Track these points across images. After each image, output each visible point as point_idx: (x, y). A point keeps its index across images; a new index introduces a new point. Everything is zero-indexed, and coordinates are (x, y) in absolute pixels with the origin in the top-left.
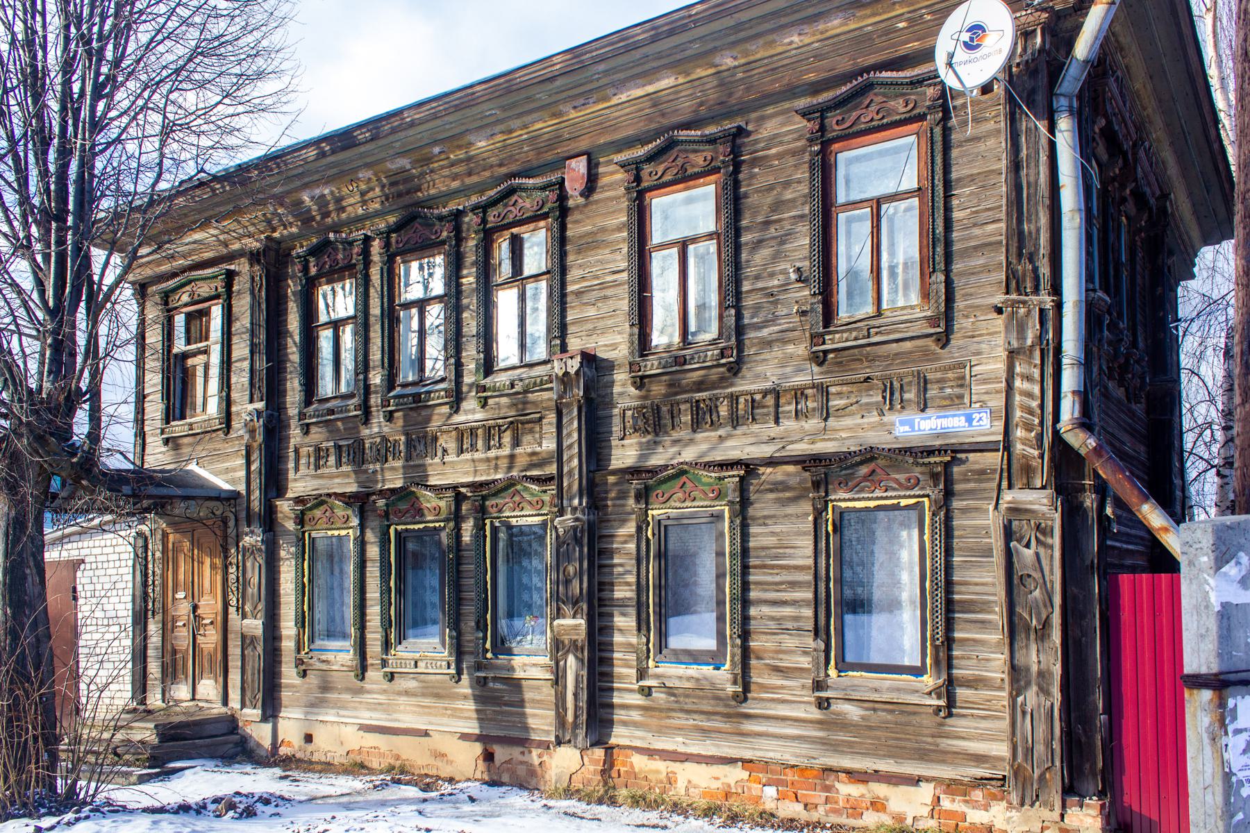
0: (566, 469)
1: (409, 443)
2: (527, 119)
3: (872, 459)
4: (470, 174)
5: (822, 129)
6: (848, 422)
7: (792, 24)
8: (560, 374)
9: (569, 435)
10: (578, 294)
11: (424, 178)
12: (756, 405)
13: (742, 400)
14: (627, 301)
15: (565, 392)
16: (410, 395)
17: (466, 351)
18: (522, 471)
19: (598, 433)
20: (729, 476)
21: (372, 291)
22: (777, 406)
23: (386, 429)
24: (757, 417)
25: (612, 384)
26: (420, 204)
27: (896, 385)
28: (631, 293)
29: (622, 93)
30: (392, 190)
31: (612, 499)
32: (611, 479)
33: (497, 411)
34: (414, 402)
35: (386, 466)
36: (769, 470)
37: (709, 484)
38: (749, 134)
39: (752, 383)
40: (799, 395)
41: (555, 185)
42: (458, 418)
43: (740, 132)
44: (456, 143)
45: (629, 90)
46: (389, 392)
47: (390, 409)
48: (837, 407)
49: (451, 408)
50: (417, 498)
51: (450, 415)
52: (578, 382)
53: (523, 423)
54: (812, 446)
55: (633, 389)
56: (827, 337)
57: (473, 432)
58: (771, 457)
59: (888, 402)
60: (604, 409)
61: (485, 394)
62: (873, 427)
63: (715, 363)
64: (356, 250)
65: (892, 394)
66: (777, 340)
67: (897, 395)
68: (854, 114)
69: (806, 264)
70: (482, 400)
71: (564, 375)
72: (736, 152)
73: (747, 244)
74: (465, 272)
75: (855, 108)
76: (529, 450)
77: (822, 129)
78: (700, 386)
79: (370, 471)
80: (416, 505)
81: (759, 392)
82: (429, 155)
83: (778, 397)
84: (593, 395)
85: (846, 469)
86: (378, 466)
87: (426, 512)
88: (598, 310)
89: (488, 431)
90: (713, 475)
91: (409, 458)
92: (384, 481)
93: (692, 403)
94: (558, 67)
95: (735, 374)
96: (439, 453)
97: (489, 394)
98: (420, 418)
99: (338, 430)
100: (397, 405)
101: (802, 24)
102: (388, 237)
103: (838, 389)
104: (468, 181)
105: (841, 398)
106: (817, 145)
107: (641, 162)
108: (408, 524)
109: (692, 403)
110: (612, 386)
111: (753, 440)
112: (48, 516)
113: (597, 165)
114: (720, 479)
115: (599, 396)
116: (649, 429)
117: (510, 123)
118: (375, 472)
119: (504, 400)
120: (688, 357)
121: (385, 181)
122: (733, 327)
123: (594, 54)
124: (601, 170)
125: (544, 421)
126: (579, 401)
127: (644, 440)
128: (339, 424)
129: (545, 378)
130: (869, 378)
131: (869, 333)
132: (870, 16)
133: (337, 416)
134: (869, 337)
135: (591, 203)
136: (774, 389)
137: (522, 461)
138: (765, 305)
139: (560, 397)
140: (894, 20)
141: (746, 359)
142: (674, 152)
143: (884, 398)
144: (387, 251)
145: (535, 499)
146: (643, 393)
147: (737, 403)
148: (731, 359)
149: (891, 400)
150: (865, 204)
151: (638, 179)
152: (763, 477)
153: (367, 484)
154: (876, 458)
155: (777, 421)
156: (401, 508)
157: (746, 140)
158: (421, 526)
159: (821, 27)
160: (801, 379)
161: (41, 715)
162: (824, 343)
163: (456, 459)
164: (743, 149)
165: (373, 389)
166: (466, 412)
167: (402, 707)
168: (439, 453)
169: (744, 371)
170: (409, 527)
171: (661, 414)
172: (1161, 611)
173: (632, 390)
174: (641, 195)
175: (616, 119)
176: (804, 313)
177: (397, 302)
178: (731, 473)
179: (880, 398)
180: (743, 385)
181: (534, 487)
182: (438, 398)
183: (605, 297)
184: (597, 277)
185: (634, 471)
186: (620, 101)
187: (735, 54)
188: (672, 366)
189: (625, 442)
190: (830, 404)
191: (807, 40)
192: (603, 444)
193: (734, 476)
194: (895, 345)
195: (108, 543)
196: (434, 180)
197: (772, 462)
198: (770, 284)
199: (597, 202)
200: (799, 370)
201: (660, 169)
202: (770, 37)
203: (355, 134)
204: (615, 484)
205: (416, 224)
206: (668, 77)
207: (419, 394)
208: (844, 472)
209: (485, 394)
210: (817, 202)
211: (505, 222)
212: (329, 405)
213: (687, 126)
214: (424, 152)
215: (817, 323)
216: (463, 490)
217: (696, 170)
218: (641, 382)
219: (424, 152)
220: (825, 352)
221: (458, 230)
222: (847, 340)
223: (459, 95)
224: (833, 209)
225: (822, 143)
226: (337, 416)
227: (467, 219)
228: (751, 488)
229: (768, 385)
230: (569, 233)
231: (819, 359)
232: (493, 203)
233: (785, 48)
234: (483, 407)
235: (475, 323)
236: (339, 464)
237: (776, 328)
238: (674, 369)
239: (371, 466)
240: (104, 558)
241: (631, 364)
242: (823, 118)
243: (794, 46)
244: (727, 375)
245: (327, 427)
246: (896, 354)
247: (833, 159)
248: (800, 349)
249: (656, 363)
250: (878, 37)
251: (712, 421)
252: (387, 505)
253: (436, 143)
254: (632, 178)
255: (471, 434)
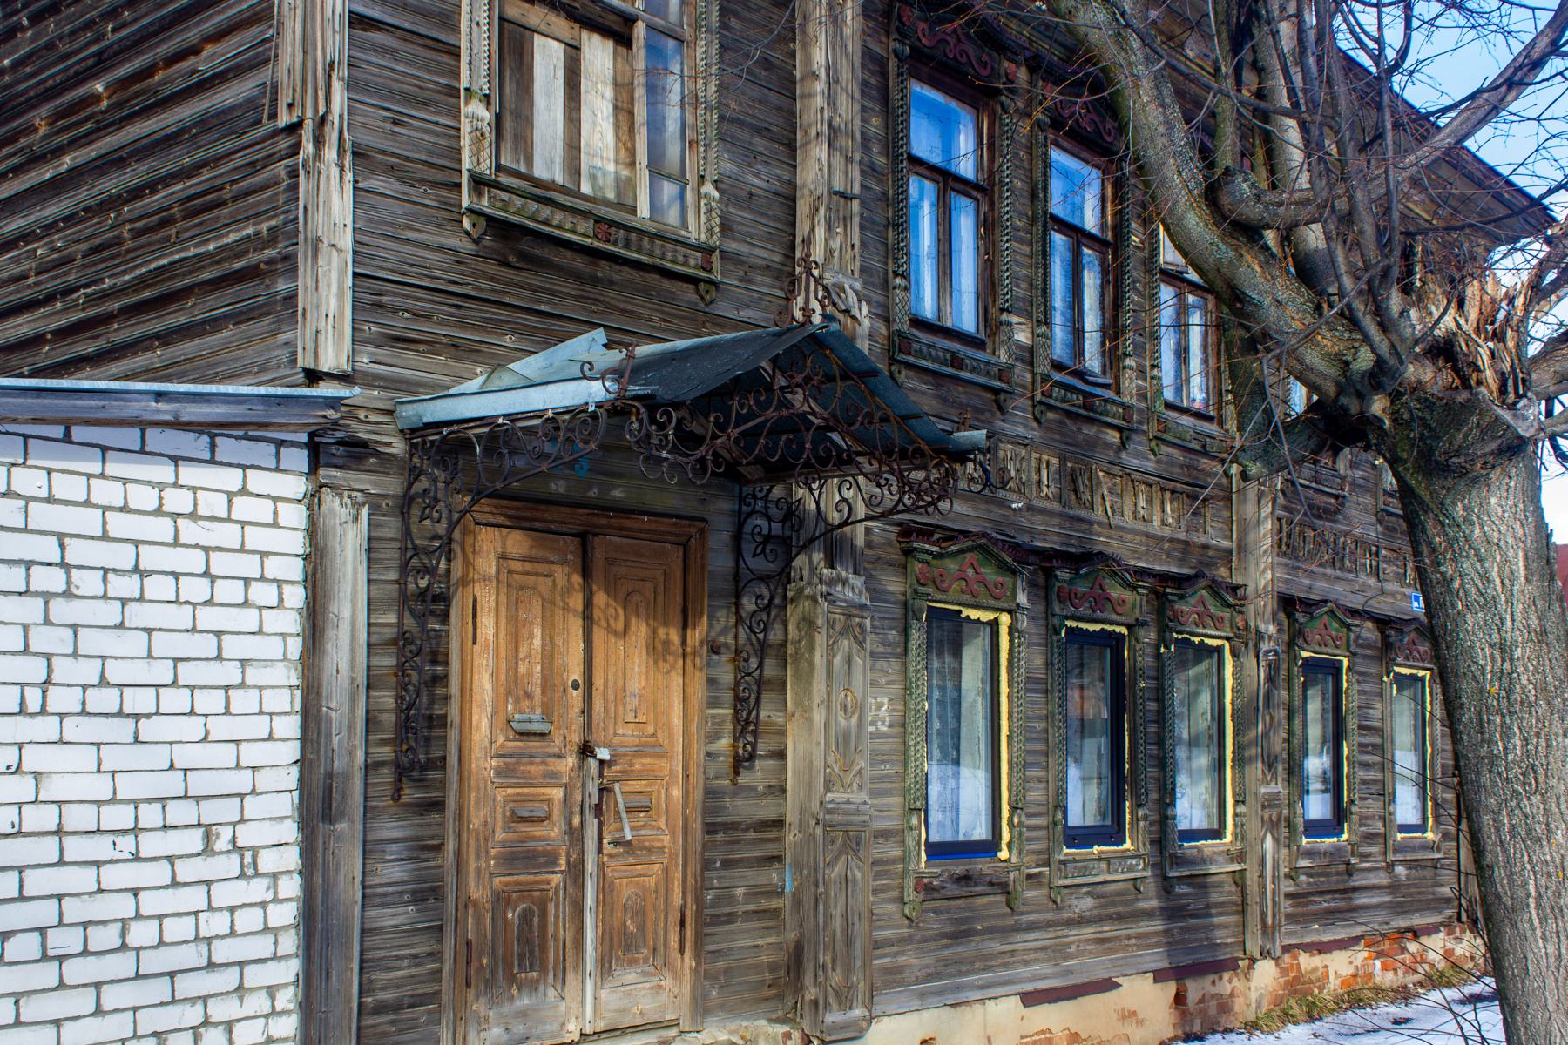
108: (1111, 623)
112: (1424, 619)
158: (1097, 627)
161: (1528, 895)
167: (1074, 949)
170: (1084, 626)
172: (528, 794)
195: (144, 498)
240: (250, 566)
245: (938, 386)
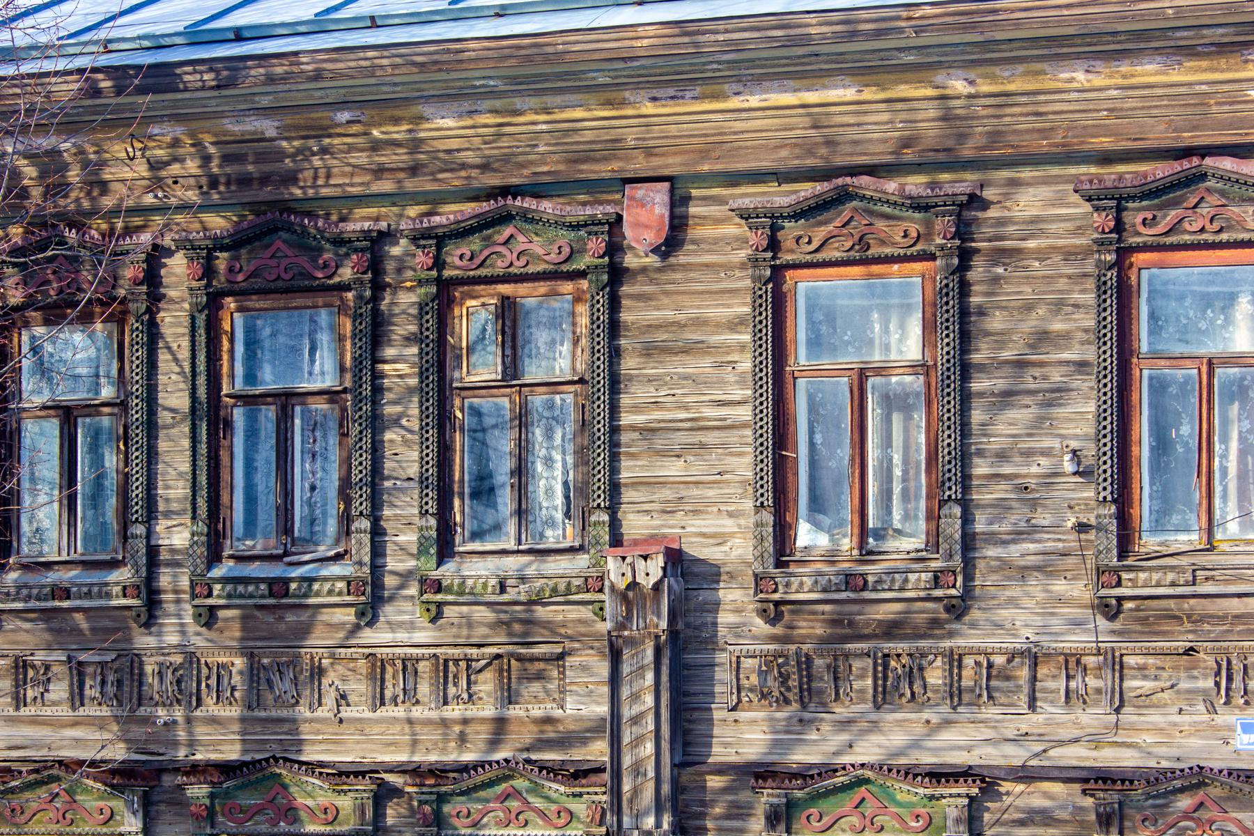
0: (627, 761)
1: (254, 673)
2: (550, 100)
3: (1201, 784)
4: (414, 170)
5: (1119, 227)
6: (1155, 718)
7: (1078, 56)
8: (622, 584)
9: (635, 697)
10: (647, 431)
11: (307, 159)
12: (994, 672)
13: (969, 661)
14: (749, 459)
15: (629, 617)
16: (263, 580)
17: (393, 505)
18: (521, 750)
19: (686, 694)
20: (951, 796)
21: (163, 357)
22: (1034, 679)
23: (199, 642)
24: (996, 694)
25: (716, 606)
26: (286, 207)
27: (1237, 666)
28: (759, 450)
29: (752, 94)
30: (228, 170)
31: (717, 818)
32: (714, 782)
33: (465, 632)
34: (271, 595)
35: (198, 713)
36: (1020, 787)
37: (911, 805)
38: (985, 205)
39: (988, 635)
40: (1072, 664)
41: (600, 223)
42: (369, 636)
43: (975, 201)
44: (389, 113)
45: (767, 91)
46: (209, 567)
47: (210, 601)
48: (1139, 692)
49: (360, 615)
50: (285, 787)
51: (357, 628)
52: (657, 601)
53: (520, 659)
54: (1094, 754)
55: (759, 621)
56: (1125, 576)
57: (408, 666)
58: (1023, 766)
59: (1223, 692)
60: (697, 651)
61: (439, 597)
62: (1197, 730)
63: (922, 594)
64: (128, 273)
65: (1230, 679)
66: (1038, 568)
67: (1237, 683)
68: (1173, 215)
69: (1090, 450)
70: (433, 608)
71: (629, 587)
72: (963, 231)
73: (981, 394)
74: (390, 352)
75: (1175, 204)
76: (537, 712)
77: (1119, 227)
78: (892, 629)
79: (160, 722)
80: (281, 801)
81: (1001, 652)
82: (325, 122)
83: (1036, 664)
84: (680, 626)
85: (1154, 797)
86: (179, 713)
87: (303, 814)
88: (686, 469)
89: (443, 669)
90: (921, 791)
91: (253, 701)
92: (192, 744)
93: (875, 658)
94: (645, 42)
95: (959, 618)
96: (330, 699)
97: (450, 598)
98: (282, 627)
99: (77, 631)
100: (229, 596)
101: (1094, 59)
102: (210, 259)
103: (1140, 660)
104: (411, 185)
105: (1145, 677)
106: (1109, 252)
107: (782, 216)
109: (875, 658)
110: (717, 611)
111: (989, 733)
113: (686, 200)
114: (931, 798)
115: (688, 625)
116: (790, 696)
117: (516, 100)
118: (170, 725)
119: (482, 613)
120: (871, 579)
121: (212, 150)
122: (958, 536)
123: (721, 37)
124: (693, 210)
125: (569, 661)
126: (657, 637)
127: (779, 715)
128: (79, 617)
129: (576, 582)
130: (1192, 649)
131: (1194, 577)
132: (1205, 70)
133: (77, 603)
134: (1194, 584)
135: (672, 268)
136: (1029, 650)
137: (520, 736)
138: (1014, 504)
139: (621, 626)
140: (1245, 85)
141: (977, 592)
142: (847, 211)
143: (1217, 684)
144: (208, 286)
145: (554, 807)
146: (778, 630)
147: (960, 667)
148: (953, 592)
149: (1228, 689)
150: (1188, 363)
151: (774, 245)
152: (1007, 800)
153: (153, 748)
154: (1206, 785)
155: (1032, 705)
156: (243, 802)
157: (980, 214)
159: (1125, 68)
160: (1077, 640)
162: (1119, 584)
163: (368, 714)
164: (973, 229)
165: (164, 556)
166: (393, 627)
168: (330, 699)
169: (975, 614)
171: (814, 671)
173: (760, 626)
174: (778, 272)
175: (735, 133)
176: (1082, 527)
177: (224, 392)
178: (954, 791)
179: (1210, 683)
180: (968, 639)
181: (555, 786)
182: (330, 593)
183: (703, 446)
184: (686, 408)
185: (760, 773)
186: (746, 105)
187: (972, 76)
188: (839, 590)
189: (742, 715)
190: (1127, 684)
191: (1098, 81)
192: (696, 715)
193: (959, 795)
194: (1236, 600)
196: (329, 169)
197: (1025, 775)
198: (1024, 470)
199: (686, 267)
200: (1077, 623)
201: (820, 234)
202: (1038, 66)
203: (178, 71)
204: (725, 790)
205: (279, 242)
206: (844, 87)
207: (286, 581)
208: (1151, 801)
209: (439, 597)
210: (1110, 349)
211: (483, 272)
212: (52, 577)
213: (872, 170)
214: (314, 115)
215: (1109, 550)
216: (390, 778)
217: (888, 251)
218: (774, 611)
219: (314, 115)
220: (1120, 600)
221: (376, 266)
222: (1158, 585)
223: (432, 48)
224: (1135, 360)
225: (1118, 250)
226: (77, 603)
227: (396, 251)
228: (987, 816)
229: (1018, 643)
230: (626, 316)
231: (1110, 609)
232: (461, 233)
233: (1060, 85)
234: (433, 621)
235: (415, 455)
236: (77, 697)
237: (1032, 547)
238: (843, 595)
239: (161, 712)
241: (758, 578)
242: (1120, 210)
243: (1075, 85)
244: (944, 616)
245: (46, 621)
246: (1236, 617)
247: (1133, 278)
248: (1079, 590)
249: (808, 582)
250: (1218, 104)
251: (913, 694)
252: (212, 796)
253: (343, 104)
254: (765, 243)
255: (405, 669)
